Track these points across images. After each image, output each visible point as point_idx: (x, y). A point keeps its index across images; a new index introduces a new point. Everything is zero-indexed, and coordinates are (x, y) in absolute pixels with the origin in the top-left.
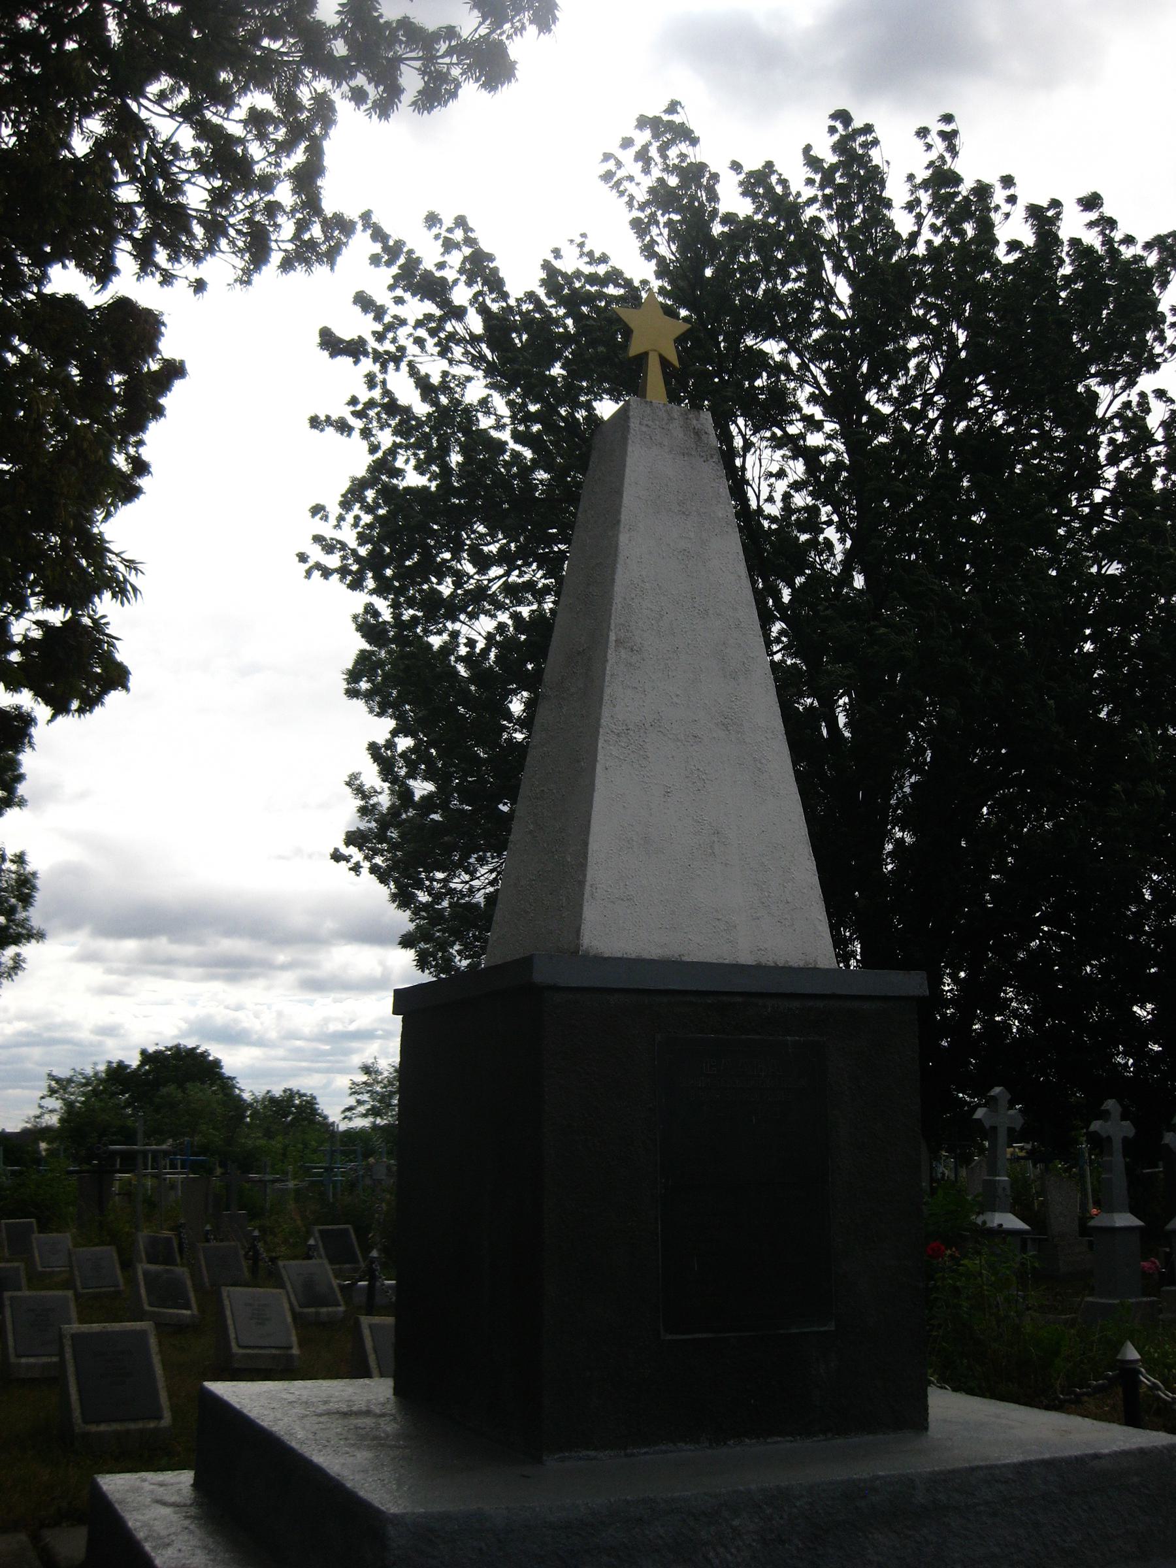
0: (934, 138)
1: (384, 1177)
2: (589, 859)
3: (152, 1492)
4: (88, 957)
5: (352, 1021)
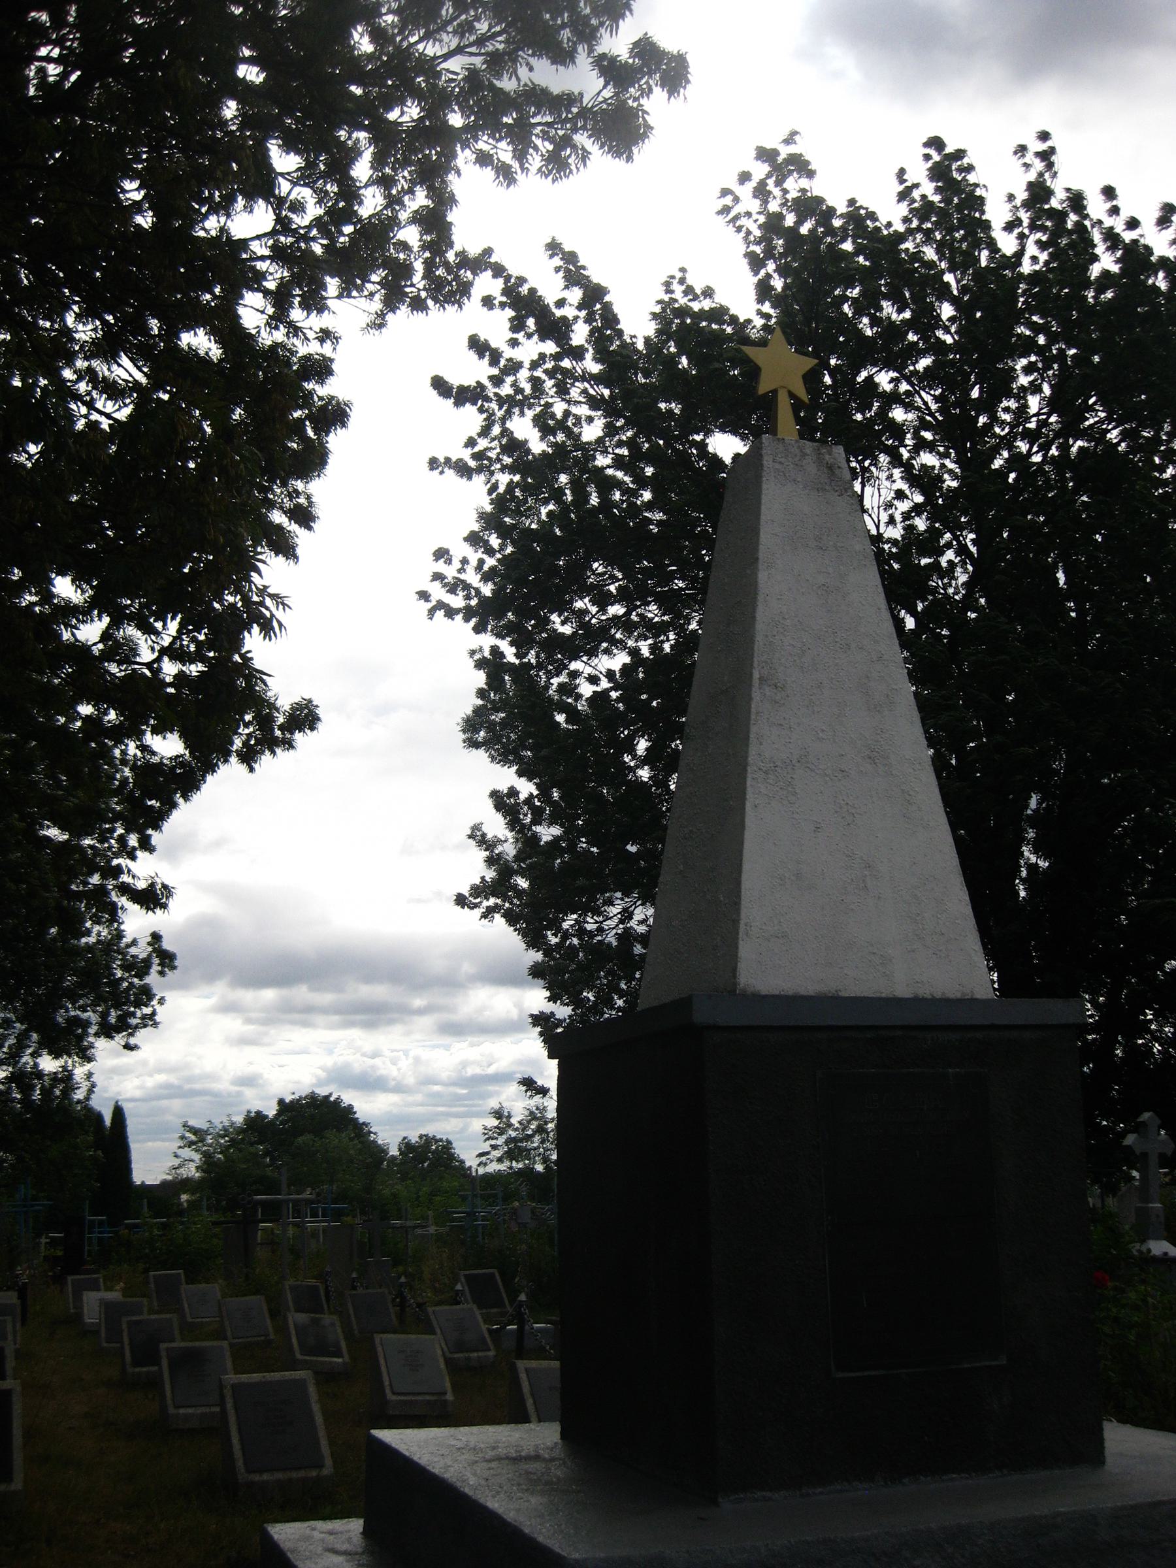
0: (1029, 158)
1: (529, 1221)
2: (743, 898)
3: (323, 1540)
4: (228, 1008)
5: (490, 1065)
